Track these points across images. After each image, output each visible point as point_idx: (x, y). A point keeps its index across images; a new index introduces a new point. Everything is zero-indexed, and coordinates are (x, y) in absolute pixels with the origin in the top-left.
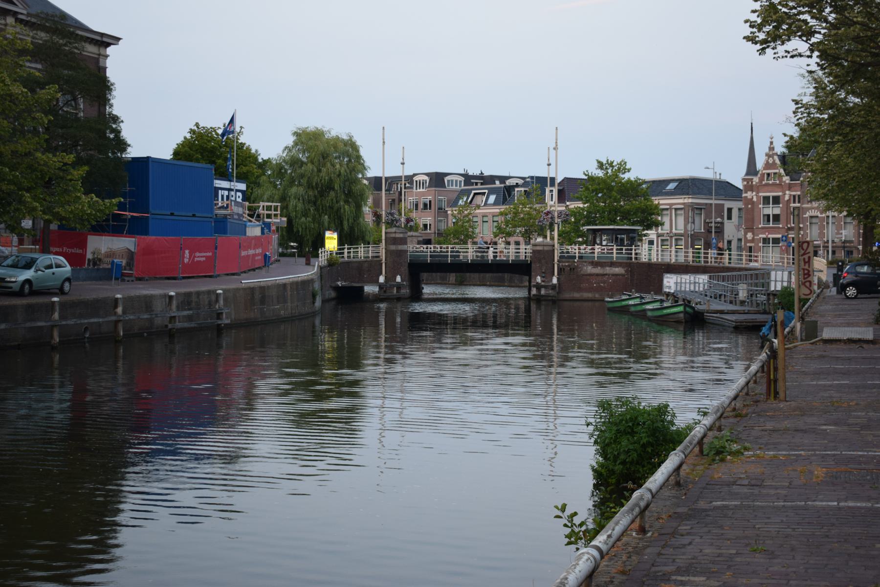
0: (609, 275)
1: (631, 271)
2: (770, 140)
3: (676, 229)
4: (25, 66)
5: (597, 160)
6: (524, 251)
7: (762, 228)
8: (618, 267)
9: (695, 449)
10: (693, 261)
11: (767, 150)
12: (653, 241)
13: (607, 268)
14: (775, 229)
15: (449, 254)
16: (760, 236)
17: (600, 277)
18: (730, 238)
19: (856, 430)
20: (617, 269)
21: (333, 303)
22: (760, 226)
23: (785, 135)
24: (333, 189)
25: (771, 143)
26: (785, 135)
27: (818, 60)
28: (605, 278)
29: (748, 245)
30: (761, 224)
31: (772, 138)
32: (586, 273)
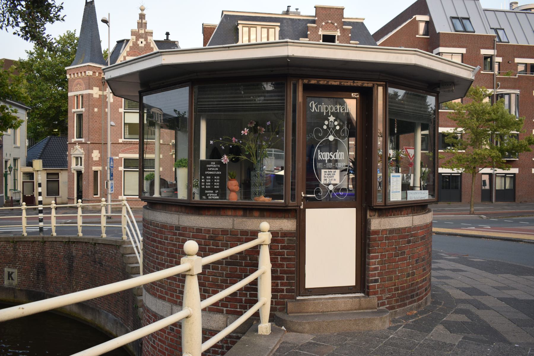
2: (140, 12)
5: (202, 343)
7: (124, 143)
10: (28, 233)
11: (135, 27)
12: (249, 198)
15: (273, 153)
18: (8, 157)
21: (179, 132)
22: (121, 141)
23: (75, 31)
25: (142, 17)
26: (75, 31)
29: (94, 168)
30: (74, 138)
31: (142, 10)
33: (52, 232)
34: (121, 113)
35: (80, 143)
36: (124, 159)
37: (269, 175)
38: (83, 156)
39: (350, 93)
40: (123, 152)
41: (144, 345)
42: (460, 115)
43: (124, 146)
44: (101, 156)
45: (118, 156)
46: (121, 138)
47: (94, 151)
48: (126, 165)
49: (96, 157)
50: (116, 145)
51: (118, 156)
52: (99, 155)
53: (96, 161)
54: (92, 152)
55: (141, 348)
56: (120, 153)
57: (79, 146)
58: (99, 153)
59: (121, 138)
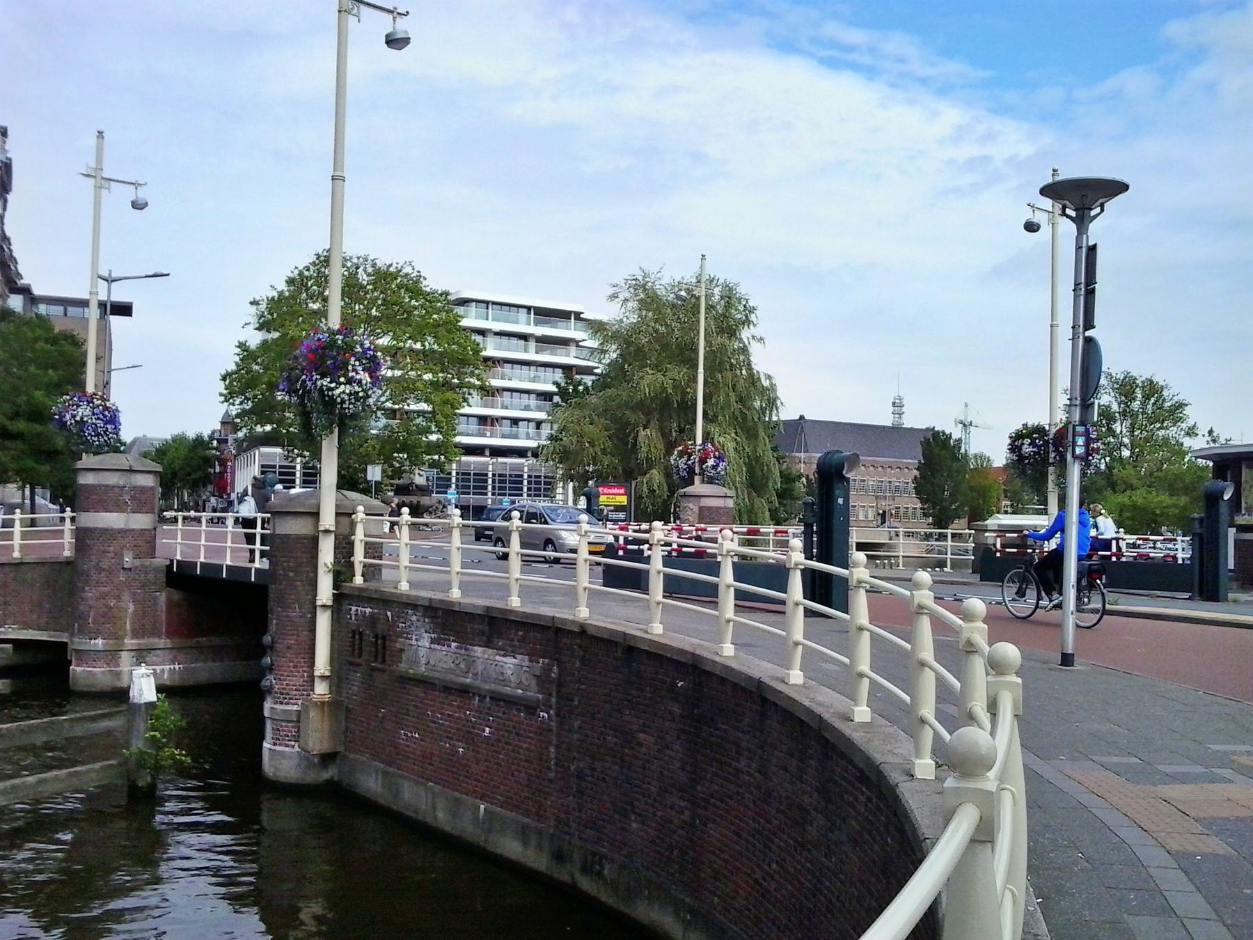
1: (560, 684)
20: (510, 664)
56: (66, 657)
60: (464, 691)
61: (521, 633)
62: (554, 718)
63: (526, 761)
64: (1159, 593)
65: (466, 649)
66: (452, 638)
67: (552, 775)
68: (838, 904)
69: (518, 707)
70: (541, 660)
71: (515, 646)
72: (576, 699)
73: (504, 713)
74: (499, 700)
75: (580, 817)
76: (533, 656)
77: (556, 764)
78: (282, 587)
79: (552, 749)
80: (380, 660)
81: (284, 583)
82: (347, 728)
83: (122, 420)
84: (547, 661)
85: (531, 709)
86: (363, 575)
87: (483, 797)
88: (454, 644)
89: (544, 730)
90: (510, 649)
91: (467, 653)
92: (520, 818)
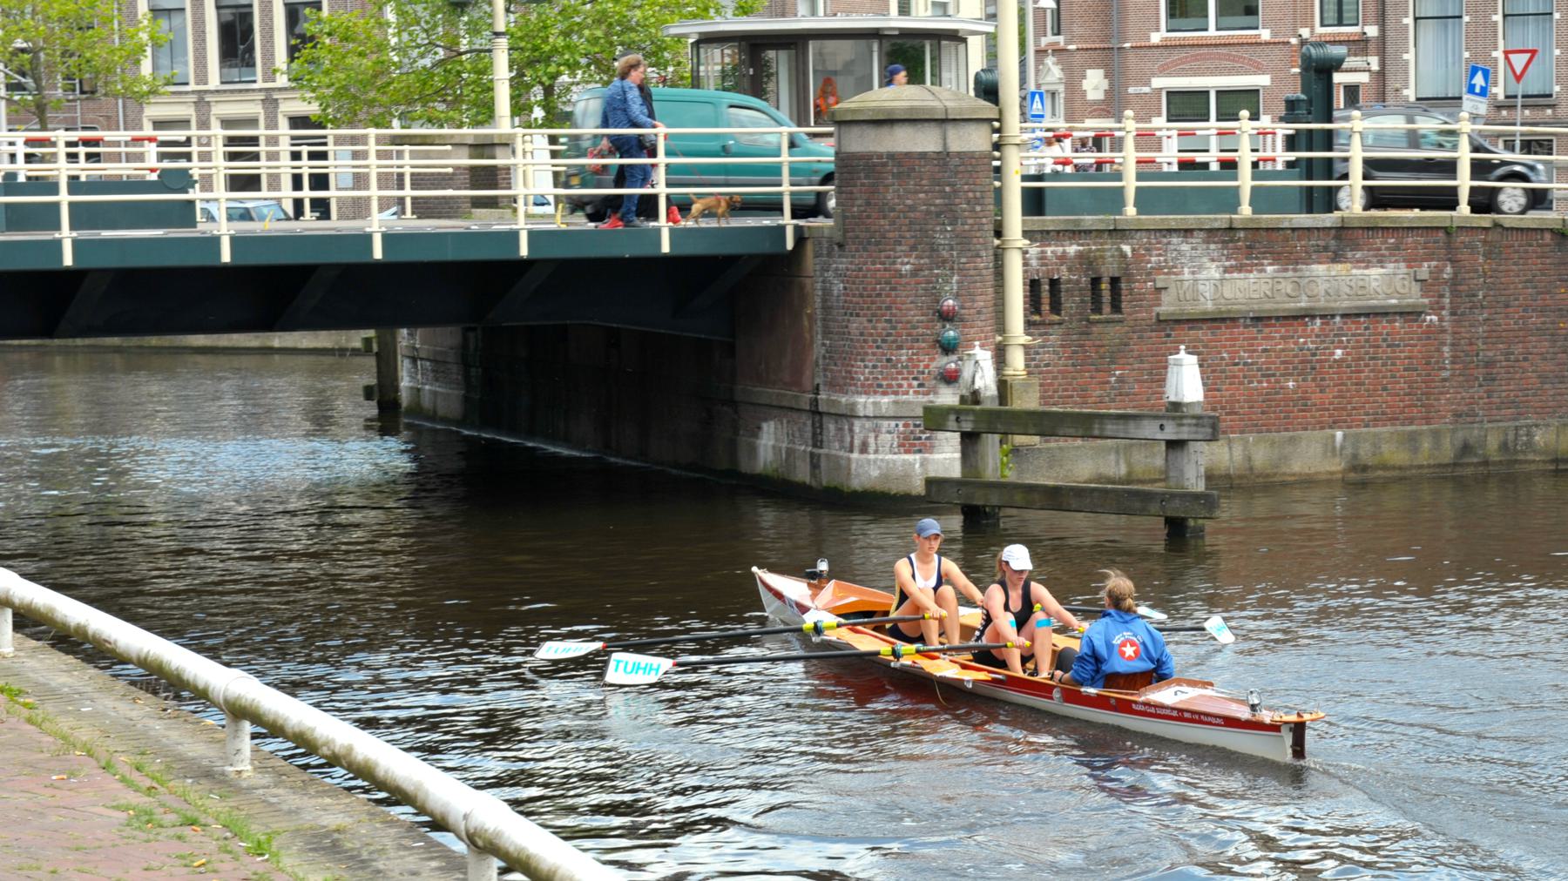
0: (1327, 317)
1: (1454, 282)
3: (1322, 25)
4: (1475, 606)
6: (305, 161)
7: (1165, 47)
8: (1381, 262)
9: (1218, 664)
13: (1319, 269)
14: (1233, 51)
16: (1159, 82)
17: (1278, 332)
19: (124, 107)
20: (1374, 276)
22: (1155, 38)
24: (840, 449)
27: (203, 227)
28: (1306, 339)
32: (1191, 309)
33: (511, 80)
34: (1558, 11)
35: (1058, 51)
36: (1168, 93)
37: (287, 670)
38: (1061, 88)
39: (242, 262)
40: (1164, 71)
41: (202, 384)
42: (460, 111)
43: (1165, 52)
44: (1111, 84)
45: (1148, 84)
46: (1158, 30)
47: (1089, 72)
48: (1173, 112)
49: (1096, 88)
50: (1142, 52)
51: (1148, 84)
52: (1105, 84)
53: (1095, 102)
54: (1084, 77)
55: (600, 814)
56: (1154, 75)
57: (1054, 59)
58: (1106, 76)
59: (1158, 30)
60: (1300, 317)
61: (1392, 241)
62: (1447, 318)
63: (1405, 370)
64: (154, 341)
65: (1295, 270)
66: (1265, 262)
67: (1445, 374)
68: (1136, 366)
69: (1390, 318)
70: (1426, 264)
71: (1383, 255)
72: (1481, 293)
73: (1366, 329)
74: (1358, 315)
75: (1490, 403)
76: (1411, 261)
77: (1453, 363)
78: (967, 227)
79: (1446, 349)
80: (1046, 307)
81: (970, 221)
82: (863, 386)
83: (365, 733)
84: (1434, 263)
85: (1411, 314)
86: (1136, 205)
87: (1335, 424)
88: (1269, 269)
89: (1433, 333)
90: (1375, 260)
91: (1298, 274)
92: (1400, 428)
